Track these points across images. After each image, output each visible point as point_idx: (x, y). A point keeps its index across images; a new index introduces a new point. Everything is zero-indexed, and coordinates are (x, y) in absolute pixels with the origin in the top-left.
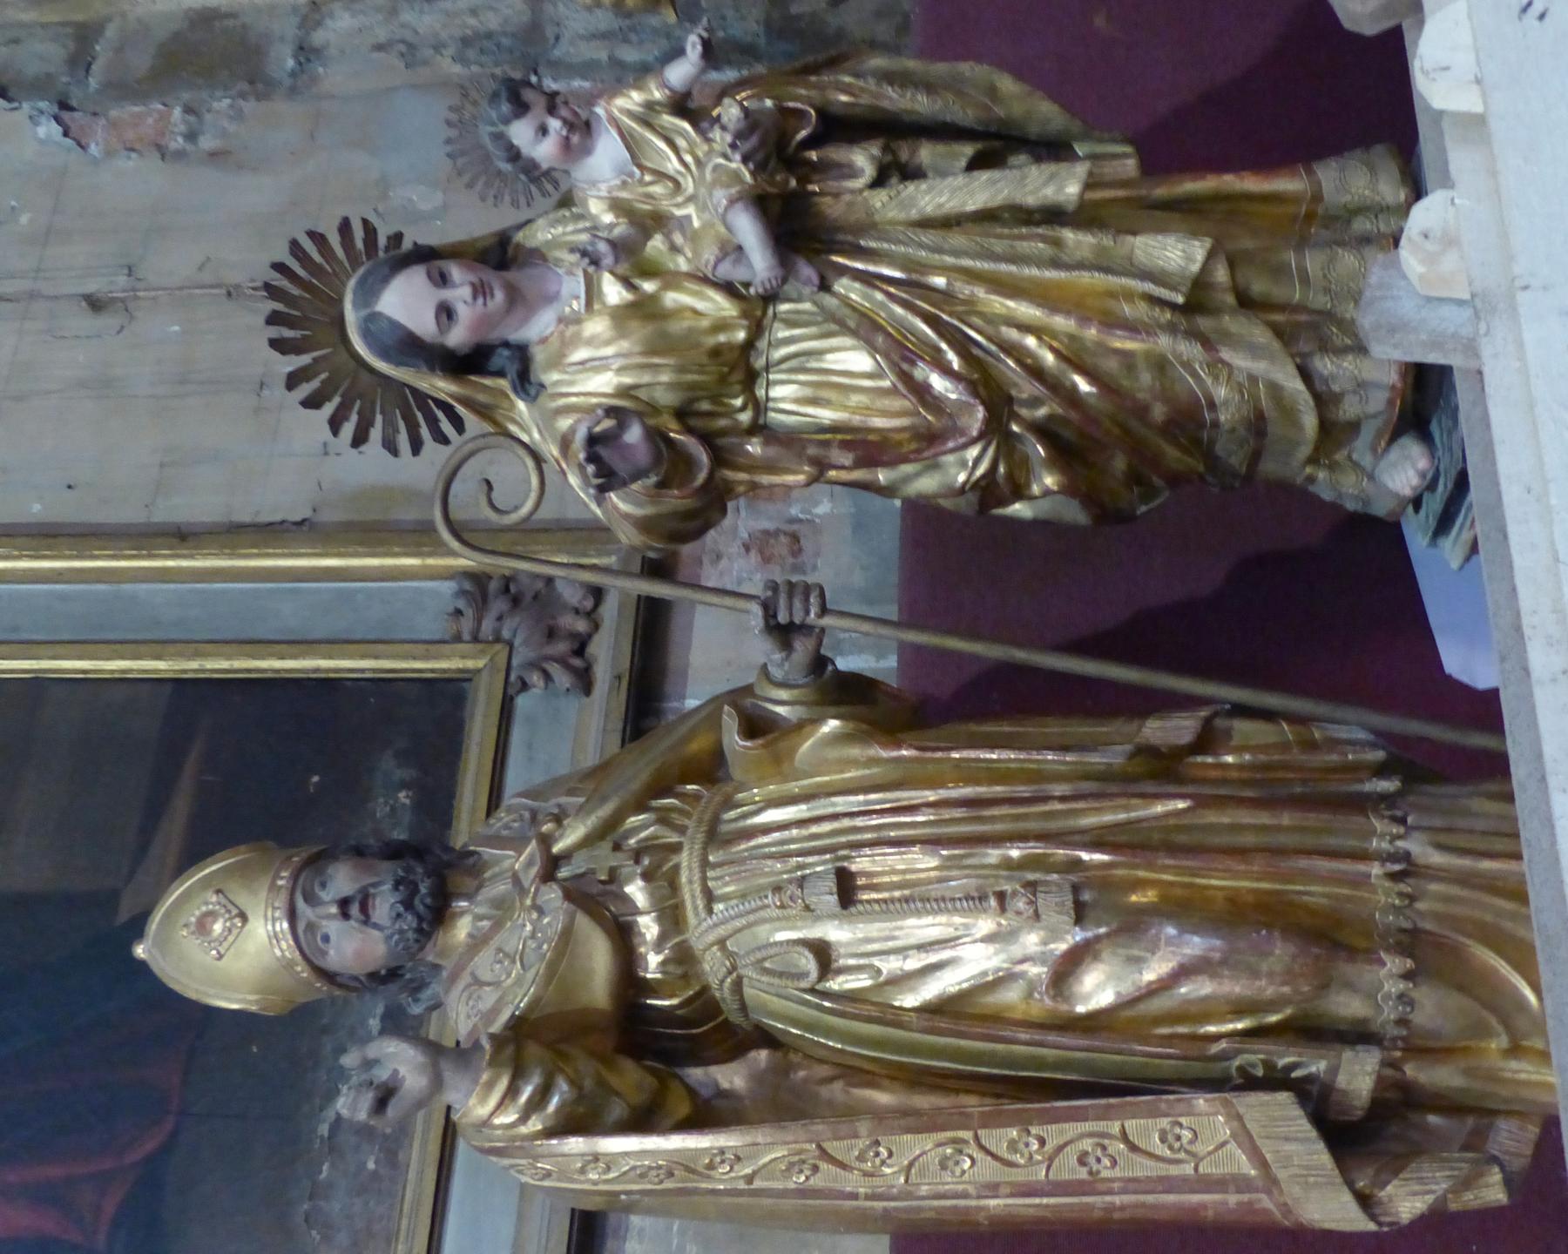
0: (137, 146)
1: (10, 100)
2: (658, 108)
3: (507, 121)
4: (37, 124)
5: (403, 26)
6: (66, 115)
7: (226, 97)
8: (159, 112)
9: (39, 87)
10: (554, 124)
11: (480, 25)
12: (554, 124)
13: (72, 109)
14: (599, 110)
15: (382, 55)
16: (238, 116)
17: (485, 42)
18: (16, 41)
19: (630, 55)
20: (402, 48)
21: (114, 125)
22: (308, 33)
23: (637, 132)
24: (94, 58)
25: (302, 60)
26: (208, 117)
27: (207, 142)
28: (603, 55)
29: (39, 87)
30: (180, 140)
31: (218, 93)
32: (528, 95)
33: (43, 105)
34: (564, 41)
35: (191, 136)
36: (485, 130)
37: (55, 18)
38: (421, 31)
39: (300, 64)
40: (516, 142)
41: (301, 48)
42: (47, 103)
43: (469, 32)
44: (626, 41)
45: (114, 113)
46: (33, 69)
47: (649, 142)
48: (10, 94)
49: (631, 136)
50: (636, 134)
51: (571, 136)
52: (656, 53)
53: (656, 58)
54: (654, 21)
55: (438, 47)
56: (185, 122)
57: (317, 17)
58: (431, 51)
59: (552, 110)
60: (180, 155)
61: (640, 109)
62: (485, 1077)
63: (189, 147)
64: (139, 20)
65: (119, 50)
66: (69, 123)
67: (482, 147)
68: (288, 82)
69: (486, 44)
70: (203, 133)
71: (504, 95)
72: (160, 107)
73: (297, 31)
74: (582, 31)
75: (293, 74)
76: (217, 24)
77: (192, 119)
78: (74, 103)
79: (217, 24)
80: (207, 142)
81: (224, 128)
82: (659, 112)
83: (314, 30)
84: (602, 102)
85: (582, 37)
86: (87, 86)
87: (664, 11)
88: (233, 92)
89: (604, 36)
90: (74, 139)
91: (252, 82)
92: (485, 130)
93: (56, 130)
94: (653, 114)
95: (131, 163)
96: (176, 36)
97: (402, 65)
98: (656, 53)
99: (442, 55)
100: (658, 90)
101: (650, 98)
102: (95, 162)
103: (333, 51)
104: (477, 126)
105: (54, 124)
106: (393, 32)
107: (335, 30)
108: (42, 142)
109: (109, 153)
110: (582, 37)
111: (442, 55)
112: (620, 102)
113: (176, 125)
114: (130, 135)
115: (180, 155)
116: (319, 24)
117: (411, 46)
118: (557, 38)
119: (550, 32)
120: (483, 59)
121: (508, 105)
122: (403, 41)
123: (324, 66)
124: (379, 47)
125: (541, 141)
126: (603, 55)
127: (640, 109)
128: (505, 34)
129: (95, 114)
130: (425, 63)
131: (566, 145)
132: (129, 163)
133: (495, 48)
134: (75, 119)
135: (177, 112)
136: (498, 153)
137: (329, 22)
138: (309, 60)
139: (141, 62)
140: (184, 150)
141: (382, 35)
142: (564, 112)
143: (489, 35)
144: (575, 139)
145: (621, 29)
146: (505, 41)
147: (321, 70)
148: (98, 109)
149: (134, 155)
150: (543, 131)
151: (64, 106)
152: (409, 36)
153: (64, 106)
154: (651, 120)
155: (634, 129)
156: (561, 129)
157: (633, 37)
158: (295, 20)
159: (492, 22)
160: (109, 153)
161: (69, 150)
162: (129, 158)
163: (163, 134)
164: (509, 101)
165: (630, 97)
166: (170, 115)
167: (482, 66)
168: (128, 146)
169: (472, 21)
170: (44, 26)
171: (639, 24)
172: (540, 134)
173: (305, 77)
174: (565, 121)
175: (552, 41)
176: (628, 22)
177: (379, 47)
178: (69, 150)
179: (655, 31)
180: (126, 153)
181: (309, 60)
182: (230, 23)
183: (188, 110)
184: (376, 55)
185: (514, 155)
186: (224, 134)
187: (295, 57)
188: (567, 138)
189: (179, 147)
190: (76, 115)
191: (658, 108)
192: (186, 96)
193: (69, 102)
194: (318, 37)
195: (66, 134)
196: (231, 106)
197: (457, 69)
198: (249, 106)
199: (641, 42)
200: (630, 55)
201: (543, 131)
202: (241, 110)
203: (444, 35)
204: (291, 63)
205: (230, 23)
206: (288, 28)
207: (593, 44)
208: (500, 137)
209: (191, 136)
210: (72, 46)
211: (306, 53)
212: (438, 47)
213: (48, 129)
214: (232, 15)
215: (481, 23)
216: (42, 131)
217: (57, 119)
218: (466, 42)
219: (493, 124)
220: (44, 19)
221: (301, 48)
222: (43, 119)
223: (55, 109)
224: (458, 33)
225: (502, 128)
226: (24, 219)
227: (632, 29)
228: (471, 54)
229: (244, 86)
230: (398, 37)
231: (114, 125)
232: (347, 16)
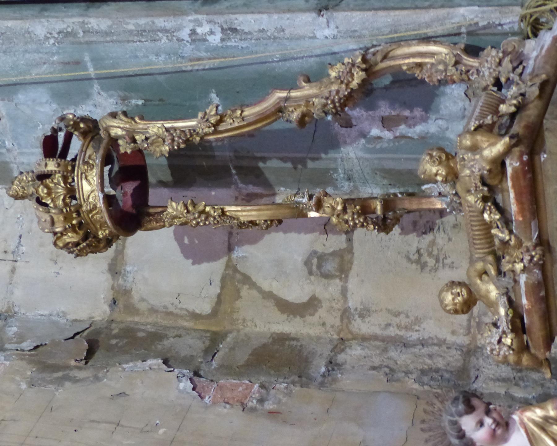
0: (231, 402)
1: (169, 367)
2: (551, 421)
3: (461, 415)
4: (180, 381)
5: (389, 358)
6: (196, 379)
7: (284, 383)
8: (247, 385)
9: (185, 362)
10: (488, 421)
11: (432, 364)
12: (488, 421)
13: (200, 376)
14: (516, 417)
15: (375, 372)
16: (289, 394)
17: (434, 374)
18: (180, 336)
19: (518, 393)
20: (387, 370)
21: (221, 388)
22: (335, 355)
23: (537, 434)
24: (218, 351)
25: (330, 369)
26: (272, 392)
27: (269, 406)
28: (502, 391)
29: (185, 362)
30: (255, 401)
31: (281, 380)
32: (475, 402)
33: (186, 371)
34: (481, 379)
35: (261, 401)
36: (447, 418)
37: (202, 327)
38: (398, 362)
39: (329, 371)
40: (464, 428)
41: (331, 362)
42: (188, 371)
43: (426, 367)
44: (516, 385)
45: (222, 382)
46: (184, 352)
47: (543, 441)
48: (170, 363)
49: (533, 434)
50: (536, 435)
51: (497, 429)
52: (534, 394)
53: (534, 397)
54: (535, 376)
55: (407, 373)
56: (259, 392)
57: (343, 347)
58: (403, 374)
59: (488, 412)
60: (253, 410)
61: (540, 420)
62: (34, 369)
63: (259, 407)
64: (246, 335)
65: (232, 349)
66: (197, 383)
67: (443, 428)
68: (320, 379)
69: (435, 375)
70: (268, 400)
71: (461, 399)
72: (247, 382)
73: (330, 353)
74: (491, 376)
75: (323, 376)
76: (287, 343)
77: (264, 391)
78: (202, 373)
79: (287, 343)
80: (269, 406)
81: (280, 399)
82: (552, 424)
83: (339, 354)
84: (518, 413)
85: (492, 379)
86: (211, 365)
87: (543, 370)
88: (289, 380)
89: (504, 380)
90: (197, 392)
91: (300, 377)
92: (447, 418)
93: (190, 385)
94: (548, 424)
95: (225, 410)
96: (264, 346)
97: (385, 380)
98: (534, 394)
99: (409, 377)
100: (553, 410)
101: (547, 414)
102: (206, 407)
103: (348, 367)
104: (441, 416)
105: (189, 382)
106: (383, 361)
107: (351, 356)
108: (180, 391)
109: (214, 403)
110: (492, 379)
111: (409, 377)
112: (529, 414)
113: (254, 394)
114: (229, 395)
115: (253, 410)
116: (343, 350)
117: (392, 370)
118: (477, 377)
119: (473, 374)
120: (432, 383)
121: (463, 405)
122: (387, 367)
123: (342, 374)
124: (374, 368)
125: (478, 430)
126: (502, 391)
127: (540, 420)
128: (446, 371)
129: (212, 381)
130: (398, 380)
131: (493, 434)
132: (225, 410)
133: (440, 378)
134: (201, 382)
135: (256, 386)
136: (452, 433)
137: (348, 350)
138: (333, 370)
139: (242, 357)
140: (256, 408)
141: (377, 361)
142: (495, 415)
143: (437, 370)
144: (499, 432)
145: (514, 378)
146: (447, 375)
147: (339, 376)
148: (214, 379)
149: (228, 406)
150: (481, 424)
151: (197, 374)
152: (391, 364)
153: (197, 374)
154: (546, 428)
155: (535, 431)
156: (492, 424)
157: (522, 384)
158: (330, 347)
159: (440, 363)
160: (214, 403)
161: (194, 398)
162: (225, 407)
163: (246, 397)
164: (464, 402)
165: (535, 412)
166: (252, 387)
167: (430, 386)
168: (226, 400)
169: (429, 361)
170: (195, 330)
171: (526, 376)
172: (479, 426)
173: (330, 378)
174: (495, 420)
175: (474, 379)
176: (519, 374)
177: (374, 368)
178: (194, 398)
179: (535, 381)
180: (224, 404)
181: (333, 370)
182: (294, 343)
183: (262, 386)
184: (371, 372)
185: (461, 435)
186: (279, 402)
187: (326, 366)
188: (494, 430)
189: (254, 406)
190: (202, 379)
191: (551, 421)
192: (263, 379)
193: (200, 372)
194: (341, 358)
195: (194, 389)
196: (287, 388)
197: (416, 386)
198: (296, 389)
199: (526, 387)
200: (518, 393)
201: (481, 424)
202: (291, 391)
203: (412, 367)
204: (323, 369)
205: (294, 343)
206: (326, 351)
207: (497, 384)
208: (455, 424)
209: (261, 401)
210: (208, 343)
211: (333, 365)
212: (407, 373)
213: (186, 385)
214: (297, 339)
215: (434, 364)
216: (182, 385)
217: (191, 379)
218: (423, 372)
219: (452, 415)
220: (196, 327)
221: (331, 362)
222: (184, 379)
223: (191, 375)
224: (420, 366)
225: (457, 418)
226: (161, 431)
227: (521, 379)
228: (426, 379)
229: (297, 379)
230: (385, 364)
231: (221, 388)
232: (359, 348)
